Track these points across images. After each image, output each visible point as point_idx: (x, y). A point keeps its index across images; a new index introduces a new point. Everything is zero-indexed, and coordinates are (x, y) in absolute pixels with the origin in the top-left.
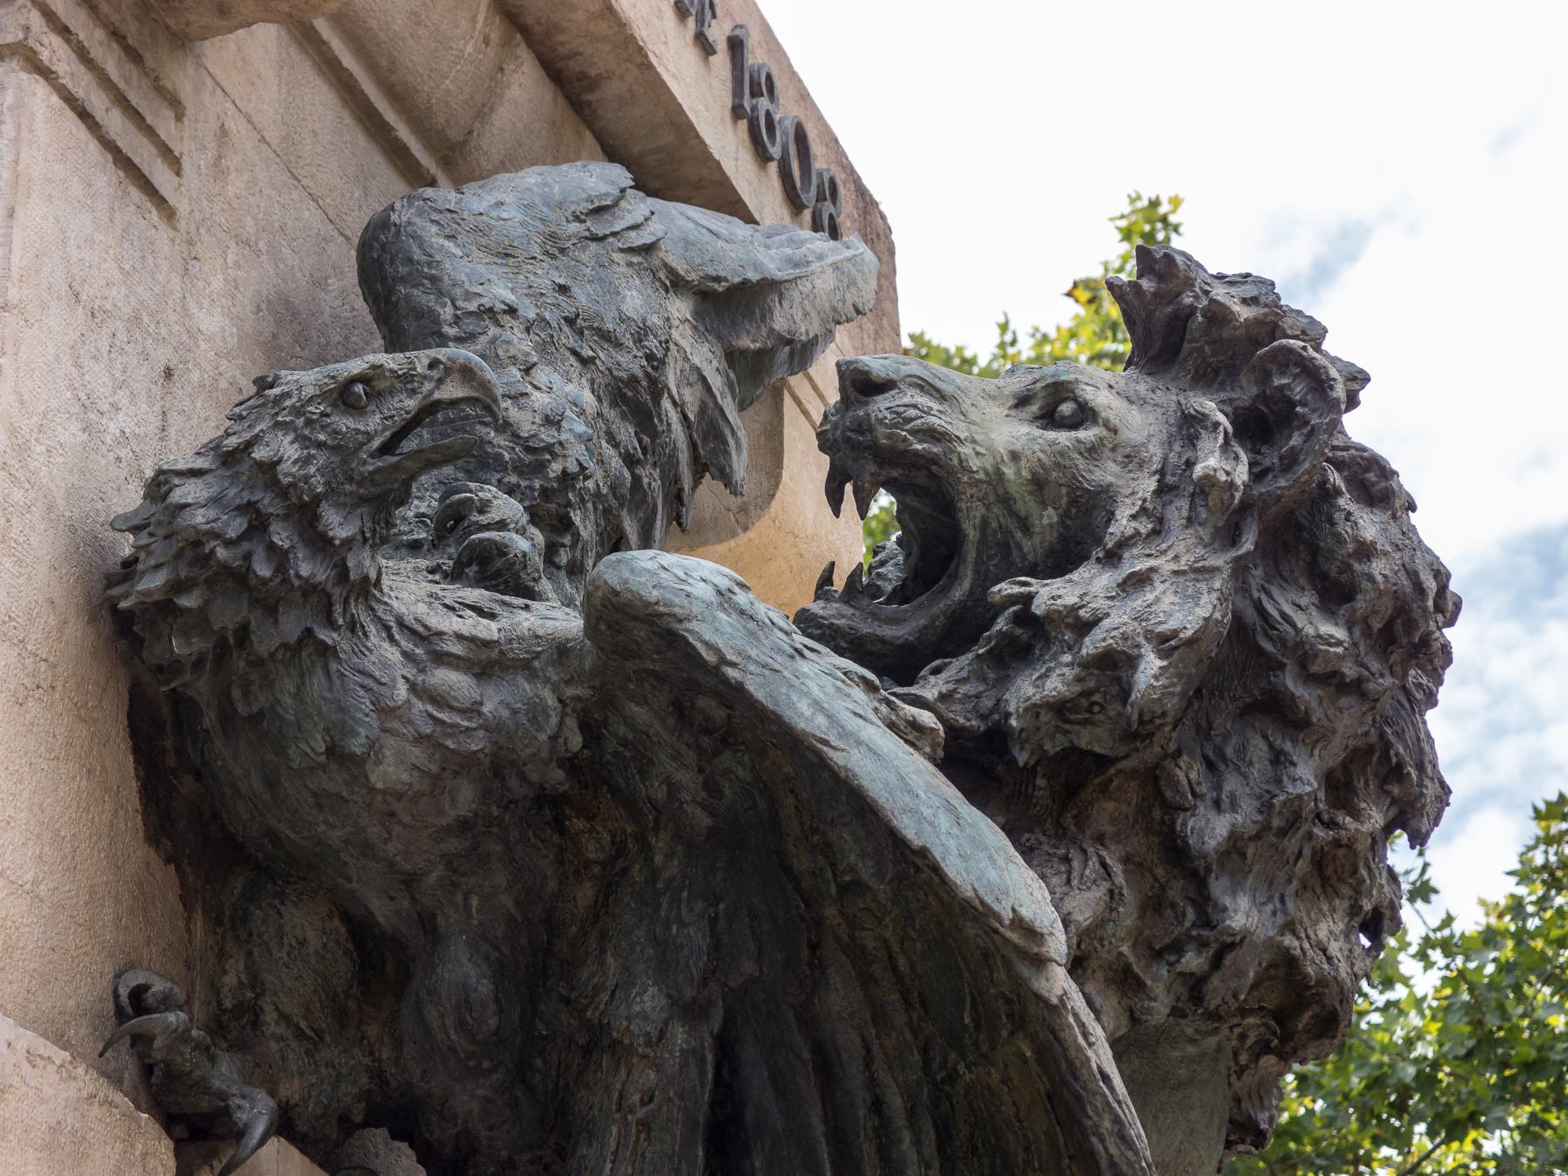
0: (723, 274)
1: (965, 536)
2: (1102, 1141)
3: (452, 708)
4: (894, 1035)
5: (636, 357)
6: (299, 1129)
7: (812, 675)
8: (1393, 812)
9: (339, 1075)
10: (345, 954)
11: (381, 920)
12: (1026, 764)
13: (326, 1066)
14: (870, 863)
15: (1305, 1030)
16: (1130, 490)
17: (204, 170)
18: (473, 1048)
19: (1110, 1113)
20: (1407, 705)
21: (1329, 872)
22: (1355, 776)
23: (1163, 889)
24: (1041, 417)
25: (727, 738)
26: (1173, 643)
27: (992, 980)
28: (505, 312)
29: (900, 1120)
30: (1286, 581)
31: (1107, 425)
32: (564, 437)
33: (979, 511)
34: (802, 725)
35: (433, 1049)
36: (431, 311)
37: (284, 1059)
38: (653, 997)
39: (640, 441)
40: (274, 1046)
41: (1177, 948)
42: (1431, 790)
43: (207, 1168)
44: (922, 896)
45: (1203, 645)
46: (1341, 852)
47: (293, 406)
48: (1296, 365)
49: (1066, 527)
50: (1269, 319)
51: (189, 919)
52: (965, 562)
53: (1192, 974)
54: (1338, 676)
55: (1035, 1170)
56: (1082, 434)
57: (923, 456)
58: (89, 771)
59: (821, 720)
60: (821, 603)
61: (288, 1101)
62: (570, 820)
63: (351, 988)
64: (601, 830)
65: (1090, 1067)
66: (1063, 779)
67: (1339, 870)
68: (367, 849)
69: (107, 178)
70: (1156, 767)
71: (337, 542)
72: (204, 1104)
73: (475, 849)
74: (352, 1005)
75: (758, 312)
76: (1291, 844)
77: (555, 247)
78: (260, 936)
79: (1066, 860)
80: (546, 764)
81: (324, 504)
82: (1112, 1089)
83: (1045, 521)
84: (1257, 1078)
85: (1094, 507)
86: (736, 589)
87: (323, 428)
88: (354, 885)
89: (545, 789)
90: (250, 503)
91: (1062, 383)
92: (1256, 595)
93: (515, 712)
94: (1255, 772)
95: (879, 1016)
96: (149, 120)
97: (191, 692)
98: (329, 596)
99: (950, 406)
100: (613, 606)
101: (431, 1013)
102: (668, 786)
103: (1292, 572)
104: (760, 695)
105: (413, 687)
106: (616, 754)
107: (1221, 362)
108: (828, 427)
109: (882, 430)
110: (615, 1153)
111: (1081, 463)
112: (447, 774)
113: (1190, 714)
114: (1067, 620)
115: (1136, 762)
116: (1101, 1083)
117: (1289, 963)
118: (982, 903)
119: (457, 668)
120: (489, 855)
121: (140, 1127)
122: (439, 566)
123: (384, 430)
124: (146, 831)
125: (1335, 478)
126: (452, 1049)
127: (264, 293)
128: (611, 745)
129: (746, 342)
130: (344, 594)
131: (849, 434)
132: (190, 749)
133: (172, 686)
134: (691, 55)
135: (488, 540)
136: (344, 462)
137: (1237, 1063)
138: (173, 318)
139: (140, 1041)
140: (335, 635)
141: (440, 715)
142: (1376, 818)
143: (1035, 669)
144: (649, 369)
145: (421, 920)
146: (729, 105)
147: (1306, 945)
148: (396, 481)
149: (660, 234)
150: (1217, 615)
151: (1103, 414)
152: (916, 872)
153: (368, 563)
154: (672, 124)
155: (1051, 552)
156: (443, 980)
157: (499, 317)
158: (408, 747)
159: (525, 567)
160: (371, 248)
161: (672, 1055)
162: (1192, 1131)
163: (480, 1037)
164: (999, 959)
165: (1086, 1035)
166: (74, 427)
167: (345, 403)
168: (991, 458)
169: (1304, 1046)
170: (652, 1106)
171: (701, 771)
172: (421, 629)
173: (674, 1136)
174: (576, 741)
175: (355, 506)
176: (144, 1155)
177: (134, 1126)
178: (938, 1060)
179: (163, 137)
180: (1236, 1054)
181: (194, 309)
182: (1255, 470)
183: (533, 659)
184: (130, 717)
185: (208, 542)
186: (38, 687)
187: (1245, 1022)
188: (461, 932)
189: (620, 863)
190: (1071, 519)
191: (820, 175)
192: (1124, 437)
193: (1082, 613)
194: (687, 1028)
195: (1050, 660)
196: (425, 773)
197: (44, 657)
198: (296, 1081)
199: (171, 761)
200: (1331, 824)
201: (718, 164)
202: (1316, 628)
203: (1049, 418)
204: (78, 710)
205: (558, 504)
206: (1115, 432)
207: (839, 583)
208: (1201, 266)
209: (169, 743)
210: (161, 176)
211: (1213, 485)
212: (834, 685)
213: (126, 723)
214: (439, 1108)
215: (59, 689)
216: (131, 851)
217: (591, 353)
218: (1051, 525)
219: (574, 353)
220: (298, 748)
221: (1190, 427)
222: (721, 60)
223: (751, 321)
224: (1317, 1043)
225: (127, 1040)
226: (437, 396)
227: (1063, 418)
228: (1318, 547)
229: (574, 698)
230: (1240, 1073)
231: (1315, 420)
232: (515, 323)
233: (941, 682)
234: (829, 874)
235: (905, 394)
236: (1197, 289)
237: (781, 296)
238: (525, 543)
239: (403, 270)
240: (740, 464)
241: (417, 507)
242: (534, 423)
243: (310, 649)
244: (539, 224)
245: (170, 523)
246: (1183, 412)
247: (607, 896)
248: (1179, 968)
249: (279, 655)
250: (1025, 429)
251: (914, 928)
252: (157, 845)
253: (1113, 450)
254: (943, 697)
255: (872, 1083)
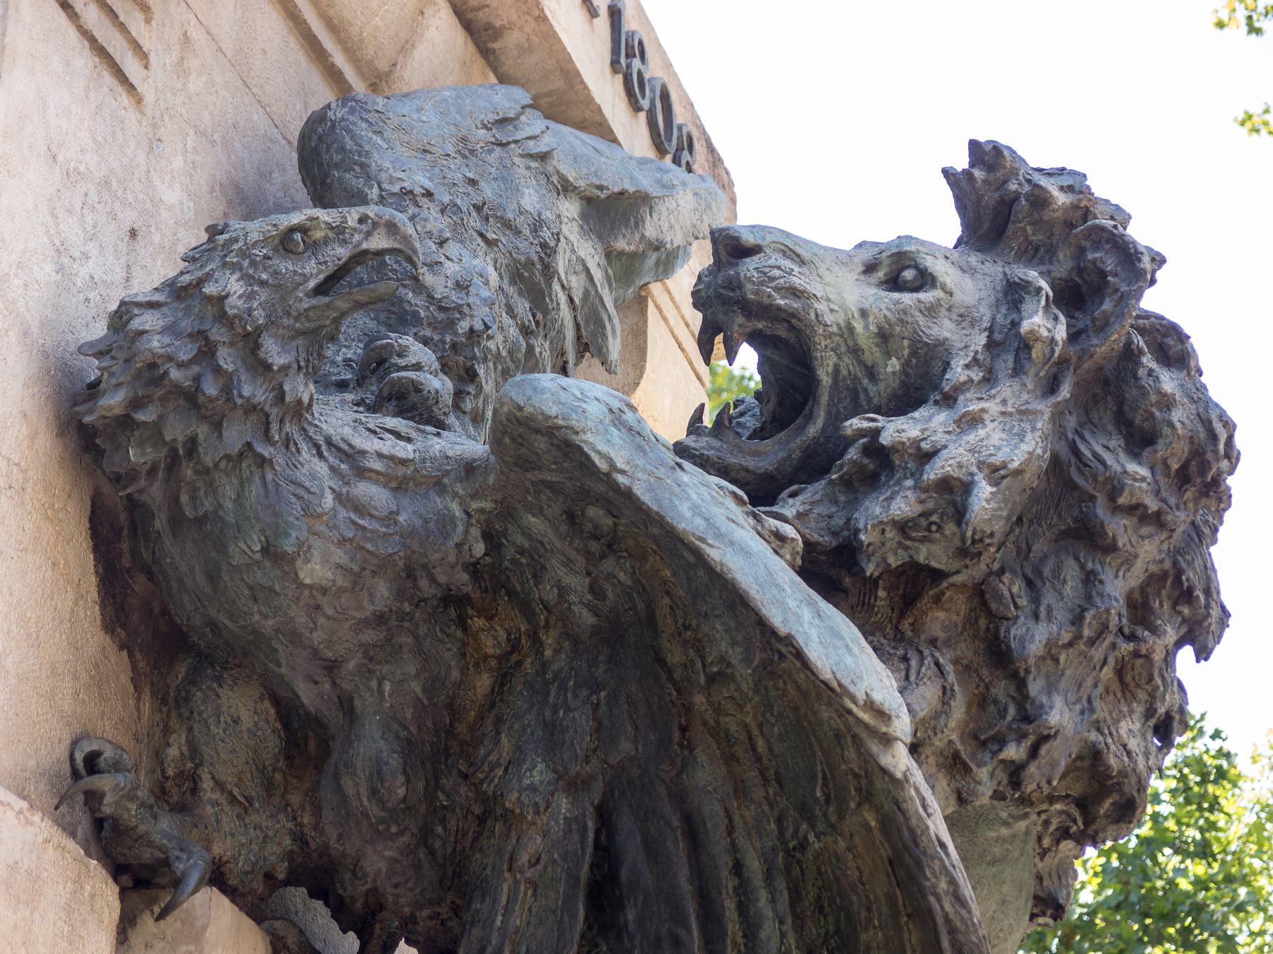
0: (605, 183)
1: (819, 382)
2: (939, 900)
3: (372, 516)
4: (753, 807)
5: (532, 243)
6: (230, 882)
7: (691, 485)
8: (1184, 630)
9: (265, 837)
10: (273, 732)
11: (306, 701)
12: (872, 575)
13: (255, 829)
14: (739, 650)
15: (1107, 816)
16: (963, 344)
17: (169, 67)
18: (383, 814)
19: (946, 876)
20: (1196, 539)
21: (1128, 679)
22: (1151, 598)
23: (987, 687)
24: (886, 282)
25: (612, 545)
26: (1002, 472)
27: (843, 757)
28: (423, 195)
29: (757, 880)
30: (1096, 427)
31: (943, 288)
32: (471, 300)
33: (832, 360)
34: (681, 526)
35: (348, 815)
36: (360, 192)
37: (218, 821)
38: (541, 772)
39: (534, 316)
40: (209, 810)
41: (1001, 742)
42: (1215, 612)
43: (148, 913)
44: (781, 684)
45: (1027, 476)
46: (1139, 662)
47: (240, 249)
48: (1107, 241)
49: (907, 375)
50: (1082, 205)
51: (138, 699)
52: (819, 404)
53: (1012, 762)
54: (1142, 508)
55: (875, 928)
56: (922, 296)
57: (785, 310)
58: (54, 564)
59: (699, 522)
60: (693, 437)
61: (220, 859)
62: (471, 619)
63: (278, 761)
64: (498, 628)
65: (929, 834)
66: (901, 592)
67: (1137, 678)
68: (294, 638)
69: (84, 60)
70: (982, 583)
71: (275, 368)
72: (147, 855)
73: (389, 640)
74: (278, 776)
75: (632, 220)
76: (1097, 653)
77: (467, 150)
78: (200, 714)
79: (905, 659)
80: (452, 567)
81: (265, 335)
82: (947, 855)
83: (889, 369)
84: (1056, 860)
85: (932, 358)
86: (625, 409)
87: (265, 268)
88: (283, 670)
89: (451, 590)
90: (200, 332)
91: (905, 253)
92: (1070, 436)
93: (426, 521)
94: (1068, 589)
95: (740, 790)
96: (122, 18)
97: (145, 498)
98: (267, 416)
99: (809, 269)
100: (517, 420)
101: (347, 783)
102: (559, 590)
103: (1100, 419)
104: (645, 498)
105: (338, 497)
106: (514, 561)
107: (1040, 241)
108: (702, 286)
109: (749, 286)
110: (506, 908)
111: (921, 320)
112: (367, 573)
113: (1012, 538)
114: (909, 451)
115: (966, 578)
116: (939, 849)
117: (1094, 755)
118: (840, 685)
119: (377, 483)
120: (401, 646)
121: (89, 871)
122: (363, 400)
123: (317, 274)
124: (103, 620)
125: (1139, 341)
126: (365, 814)
127: (218, 177)
128: (510, 552)
129: (621, 244)
130: (280, 415)
131: (721, 291)
132: (143, 549)
133: (129, 491)
134: (580, 14)
135: (406, 378)
136: (283, 299)
137: (1040, 846)
138: (139, 187)
139: (92, 798)
140: (272, 449)
141: (361, 522)
142: (1171, 635)
143: (881, 493)
144: (543, 255)
145: (341, 702)
146: (608, 61)
147: (1110, 741)
148: (328, 318)
149: (554, 145)
150: (1039, 451)
151: (941, 279)
152: (780, 659)
153: (301, 388)
154: (562, 71)
155: (894, 397)
156: (358, 754)
157: (418, 199)
158: (333, 548)
159: (437, 402)
160: (310, 138)
161: (557, 823)
162: (1004, 902)
163: (390, 804)
164: (849, 740)
165: (925, 807)
166: (49, 268)
167: (285, 249)
168: (843, 315)
169: (1104, 830)
170: (539, 867)
171: (588, 574)
172: (346, 448)
173: (558, 892)
174: (479, 548)
175: (293, 338)
176: (93, 896)
177: (84, 870)
178: (791, 831)
179: (134, 34)
180: (1039, 839)
181: (157, 181)
182: (1071, 332)
183: (443, 476)
184: (91, 520)
185: (163, 364)
186: (10, 487)
187: (1052, 808)
188: (375, 713)
189: (515, 657)
190: (911, 368)
191: (680, 128)
192: (958, 299)
193: (923, 445)
194: (570, 799)
195: (894, 485)
196: (349, 571)
197: (16, 461)
198: (228, 841)
199: (126, 562)
200: (1132, 637)
201: (599, 109)
202: (1123, 466)
203: (894, 283)
204: (46, 510)
205: (466, 358)
206: (951, 294)
207: (708, 421)
208: (1024, 160)
209: (125, 546)
210: (131, 66)
211: (1037, 340)
212: (709, 494)
213: (88, 526)
214: (352, 867)
215: (29, 490)
216: (89, 636)
217: (494, 236)
218: (894, 373)
219: (481, 235)
220: (237, 546)
221: (1014, 293)
222: (603, 22)
223: (626, 226)
224: (1115, 827)
225: (81, 798)
226: (365, 246)
227: (906, 282)
228: (1124, 398)
229: (477, 511)
230: (1043, 854)
231: (1124, 288)
232: (431, 205)
233: (798, 503)
234: (700, 665)
235: (770, 258)
236: (1021, 178)
237: (651, 208)
238: (439, 384)
239: (337, 158)
240: (615, 347)
241: (344, 354)
242: (446, 287)
243: (250, 461)
244: (453, 128)
245: (129, 348)
246: (1008, 281)
247: (502, 686)
248: (1001, 756)
249: (222, 465)
250: (873, 291)
251: (772, 715)
252: (113, 633)
253: (949, 310)
254: (799, 515)
255: (734, 848)
